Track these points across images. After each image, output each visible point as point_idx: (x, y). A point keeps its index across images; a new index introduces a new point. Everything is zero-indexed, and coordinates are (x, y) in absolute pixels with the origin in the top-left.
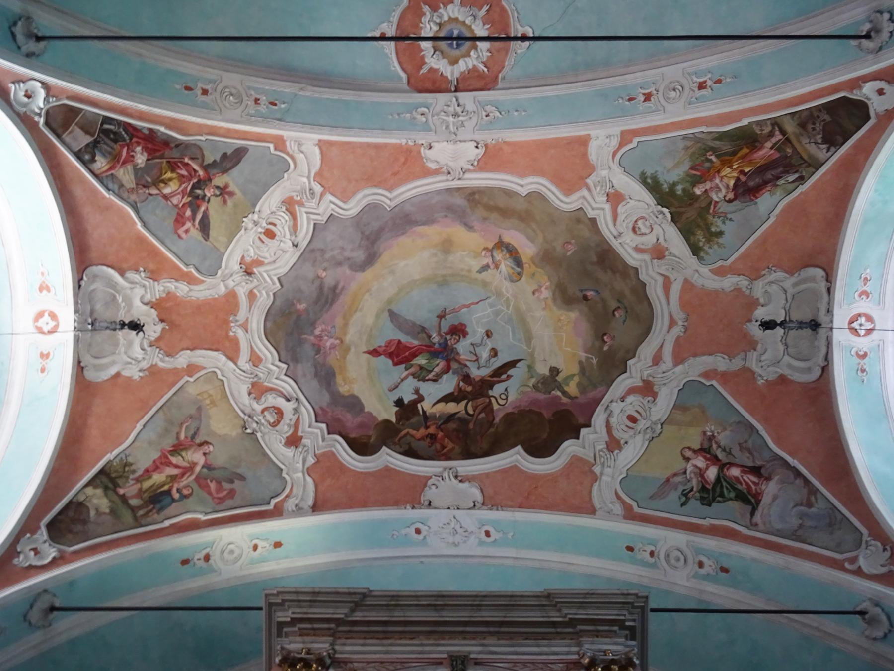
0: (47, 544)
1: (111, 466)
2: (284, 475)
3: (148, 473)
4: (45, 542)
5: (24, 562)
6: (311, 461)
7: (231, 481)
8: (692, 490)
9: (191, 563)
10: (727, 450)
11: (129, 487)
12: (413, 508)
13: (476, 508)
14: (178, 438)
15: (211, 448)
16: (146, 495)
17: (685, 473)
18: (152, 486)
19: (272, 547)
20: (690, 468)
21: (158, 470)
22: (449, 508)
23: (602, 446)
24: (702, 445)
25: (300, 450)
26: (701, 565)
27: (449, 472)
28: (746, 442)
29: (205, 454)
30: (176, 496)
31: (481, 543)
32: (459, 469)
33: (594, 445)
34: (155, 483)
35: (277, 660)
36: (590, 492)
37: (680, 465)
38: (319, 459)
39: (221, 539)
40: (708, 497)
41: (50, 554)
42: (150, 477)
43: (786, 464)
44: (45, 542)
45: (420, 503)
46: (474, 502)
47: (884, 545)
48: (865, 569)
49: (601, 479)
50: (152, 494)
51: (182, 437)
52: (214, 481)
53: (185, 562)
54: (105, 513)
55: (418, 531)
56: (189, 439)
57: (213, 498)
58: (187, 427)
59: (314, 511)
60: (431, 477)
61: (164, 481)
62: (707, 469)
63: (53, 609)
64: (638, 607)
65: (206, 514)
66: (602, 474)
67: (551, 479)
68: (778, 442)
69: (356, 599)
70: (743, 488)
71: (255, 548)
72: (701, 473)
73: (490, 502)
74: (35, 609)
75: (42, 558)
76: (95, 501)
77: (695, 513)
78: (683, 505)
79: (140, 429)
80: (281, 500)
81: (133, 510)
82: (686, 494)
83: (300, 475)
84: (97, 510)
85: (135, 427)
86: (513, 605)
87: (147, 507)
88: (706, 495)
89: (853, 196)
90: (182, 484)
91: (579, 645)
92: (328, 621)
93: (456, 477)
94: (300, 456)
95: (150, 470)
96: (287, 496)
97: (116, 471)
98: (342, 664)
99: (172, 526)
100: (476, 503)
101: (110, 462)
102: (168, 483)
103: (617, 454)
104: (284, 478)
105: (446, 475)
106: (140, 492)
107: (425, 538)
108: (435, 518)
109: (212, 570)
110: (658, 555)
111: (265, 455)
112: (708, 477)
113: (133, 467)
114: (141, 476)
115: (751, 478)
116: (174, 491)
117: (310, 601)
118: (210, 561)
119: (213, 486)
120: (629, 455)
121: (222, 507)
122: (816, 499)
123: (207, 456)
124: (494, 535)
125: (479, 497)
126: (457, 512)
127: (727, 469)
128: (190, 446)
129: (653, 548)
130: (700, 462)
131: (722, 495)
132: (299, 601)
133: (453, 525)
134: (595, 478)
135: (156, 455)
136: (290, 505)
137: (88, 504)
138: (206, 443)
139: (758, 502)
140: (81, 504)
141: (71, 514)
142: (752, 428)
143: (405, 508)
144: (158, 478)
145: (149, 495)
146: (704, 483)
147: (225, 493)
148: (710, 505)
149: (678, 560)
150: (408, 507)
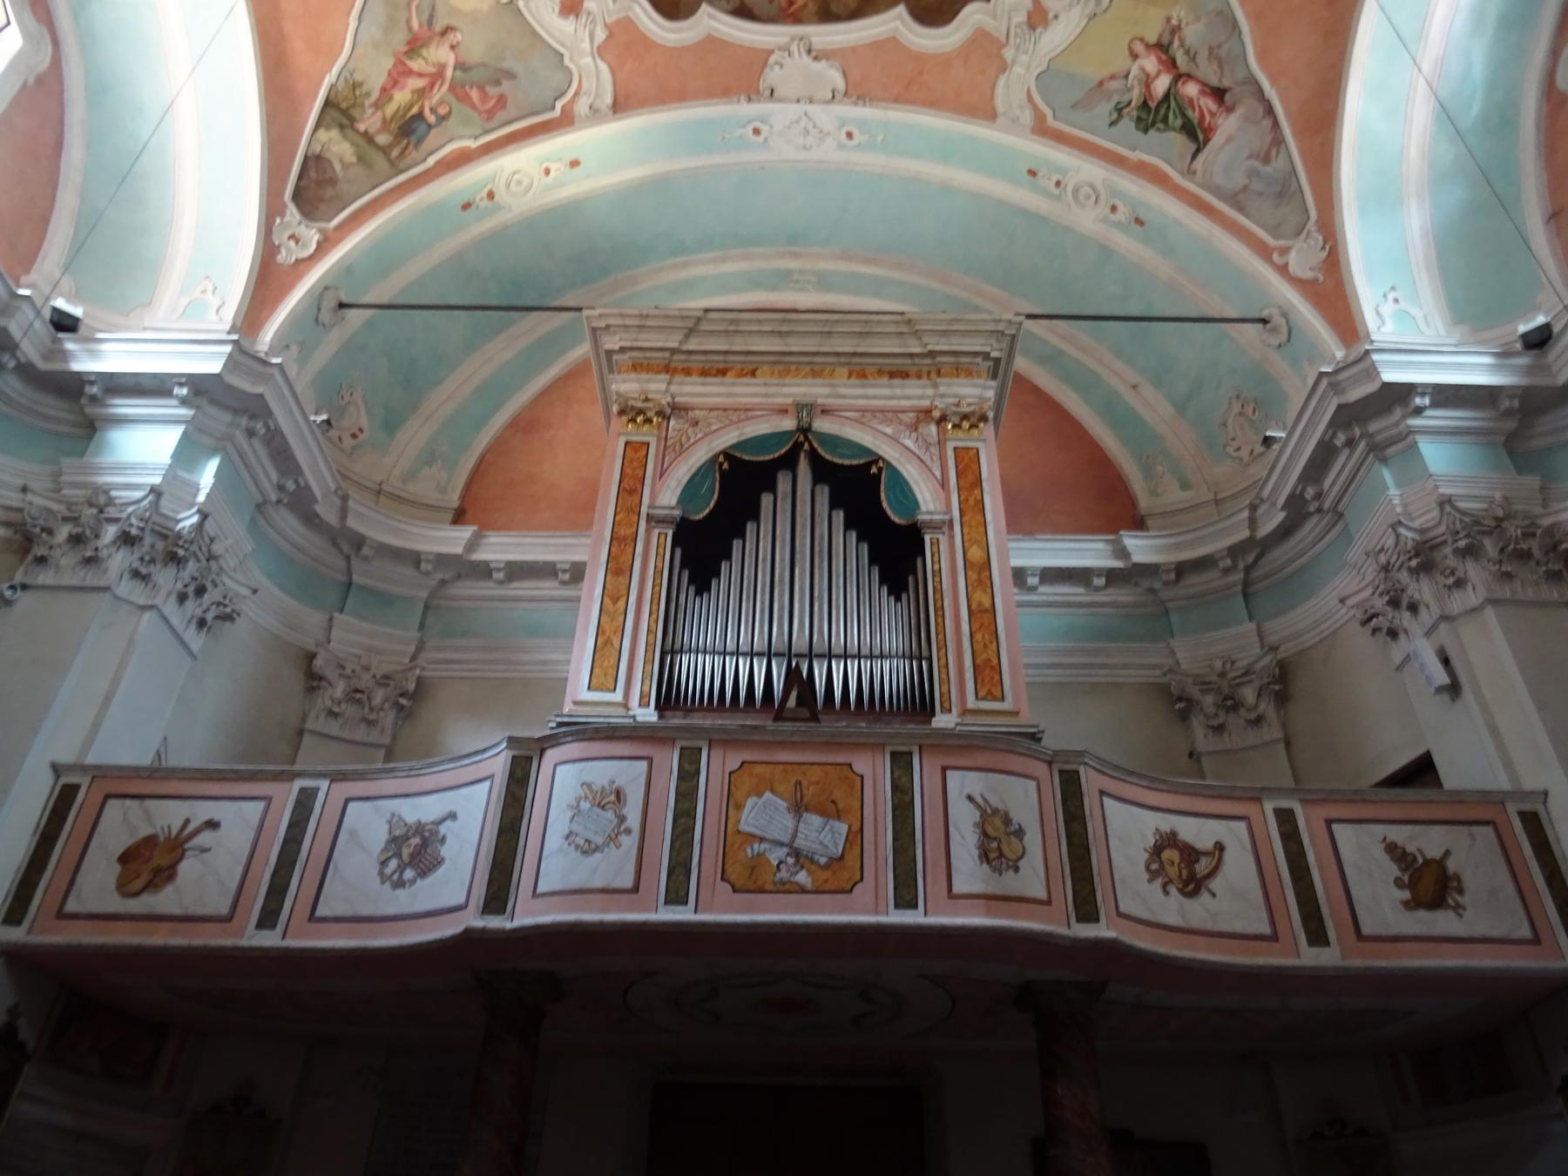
0: (303, 227)
1: (337, 91)
2: (567, 62)
3: (386, 92)
4: (300, 223)
5: (289, 258)
6: (601, 35)
7: (498, 83)
8: (1129, 103)
9: (473, 207)
10: (1192, 53)
11: (369, 118)
12: (749, 100)
13: (836, 101)
14: (410, 29)
15: (459, 37)
16: (394, 126)
17: (1127, 76)
18: (397, 112)
19: (568, 167)
20: (1135, 71)
21: (398, 86)
22: (798, 101)
23: (1020, 18)
24: (1160, 37)
25: (584, 20)
26: (1114, 209)
27: (799, 46)
28: (1219, 46)
29: (453, 47)
30: (432, 119)
31: (840, 146)
32: (815, 40)
33: (1009, 15)
34: (399, 107)
35: (615, 408)
36: (993, 88)
37: (1121, 62)
38: (611, 30)
39: (502, 170)
40: (1147, 120)
41: (312, 238)
42: (391, 98)
43: (1260, 92)
44: (300, 223)
45: (758, 92)
46: (833, 92)
47: (1325, 242)
48: (1294, 268)
49: (1011, 70)
50: (401, 122)
51: (415, 24)
52: (474, 88)
53: (466, 206)
54: (352, 164)
55: (757, 131)
56: (426, 27)
57: (480, 113)
58: (418, 8)
59: (615, 112)
60: (772, 52)
61: (409, 101)
62: (1157, 76)
63: (342, 306)
64: (1007, 335)
65: (476, 138)
66: (1014, 62)
67: (942, 61)
68: (1262, 57)
69: (690, 324)
70: (1194, 116)
71: (547, 172)
72: (1147, 81)
73: (856, 92)
74: (323, 310)
75: (305, 246)
76: (335, 149)
77: (1127, 140)
78: (1112, 124)
79: (356, 26)
80: (569, 102)
81: (385, 151)
82: (1119, 110)
83: (589, 60)
84: (341, 161)
85: (348, 25)
86: (868, 333)
87: (399, 143)
88: (1144, 116)
89: (1349, 47)
90: (435, 100)
91: (935, 386)
92: (662, 349)
93: (809, 51)
94: (584, 32)
95: (388, 86)
96: (576, 94)
97: (345, 99)
98: (683, 413)
99: (438, 163)
100: (836, 93)
101: (332, 87)
102: (417, 102)
103: (1041, 33)
104: (567, 67)
105: (794, 48)
106: (385, 123)
107: (766, 140)
108: (780, 114)
109: (499, 208)
110: (1066, 185)
111: (534, 33)
112: (1155, 90)
113: (365, 89)
114: (379, 99)
115: (1208, 104)
116: (427, 112)
117: (639, 327)
118: (495, 199)
119: (474, 94)
120: (1055, 38)
121: (493, 123)
122: (1278, 153)
123: (457, 49)
124: (858, 138)
125: (840, 84)
126: (812, 109)
127: (1184, 83)
128: (431, 38)
129: (1061, 179)
130: (1150, 63)
131: (1165, 120)
132: (626, 326)
133: (803, 123)
134: (1003, 67)
135: (388, 63)
136: (582, 107)
137: (328, 155)
138: (447, 30)
139: (1207, 141)
140: (319, 157)
141: (313, 174)
142: (1235, 25)
143: (739, 101)
144: (401, 97)
145: (397, 126)
146: (1147, 98)
147: (492, 102)
148: (1146, 131)
149: (1088, 197)
150: (742, 97)
